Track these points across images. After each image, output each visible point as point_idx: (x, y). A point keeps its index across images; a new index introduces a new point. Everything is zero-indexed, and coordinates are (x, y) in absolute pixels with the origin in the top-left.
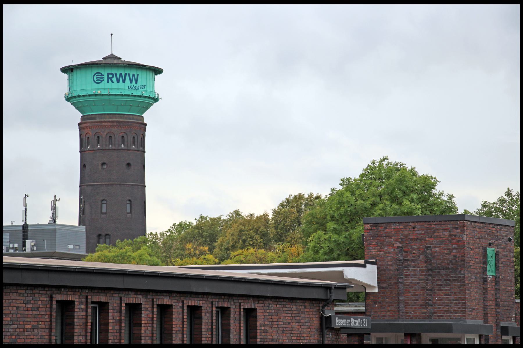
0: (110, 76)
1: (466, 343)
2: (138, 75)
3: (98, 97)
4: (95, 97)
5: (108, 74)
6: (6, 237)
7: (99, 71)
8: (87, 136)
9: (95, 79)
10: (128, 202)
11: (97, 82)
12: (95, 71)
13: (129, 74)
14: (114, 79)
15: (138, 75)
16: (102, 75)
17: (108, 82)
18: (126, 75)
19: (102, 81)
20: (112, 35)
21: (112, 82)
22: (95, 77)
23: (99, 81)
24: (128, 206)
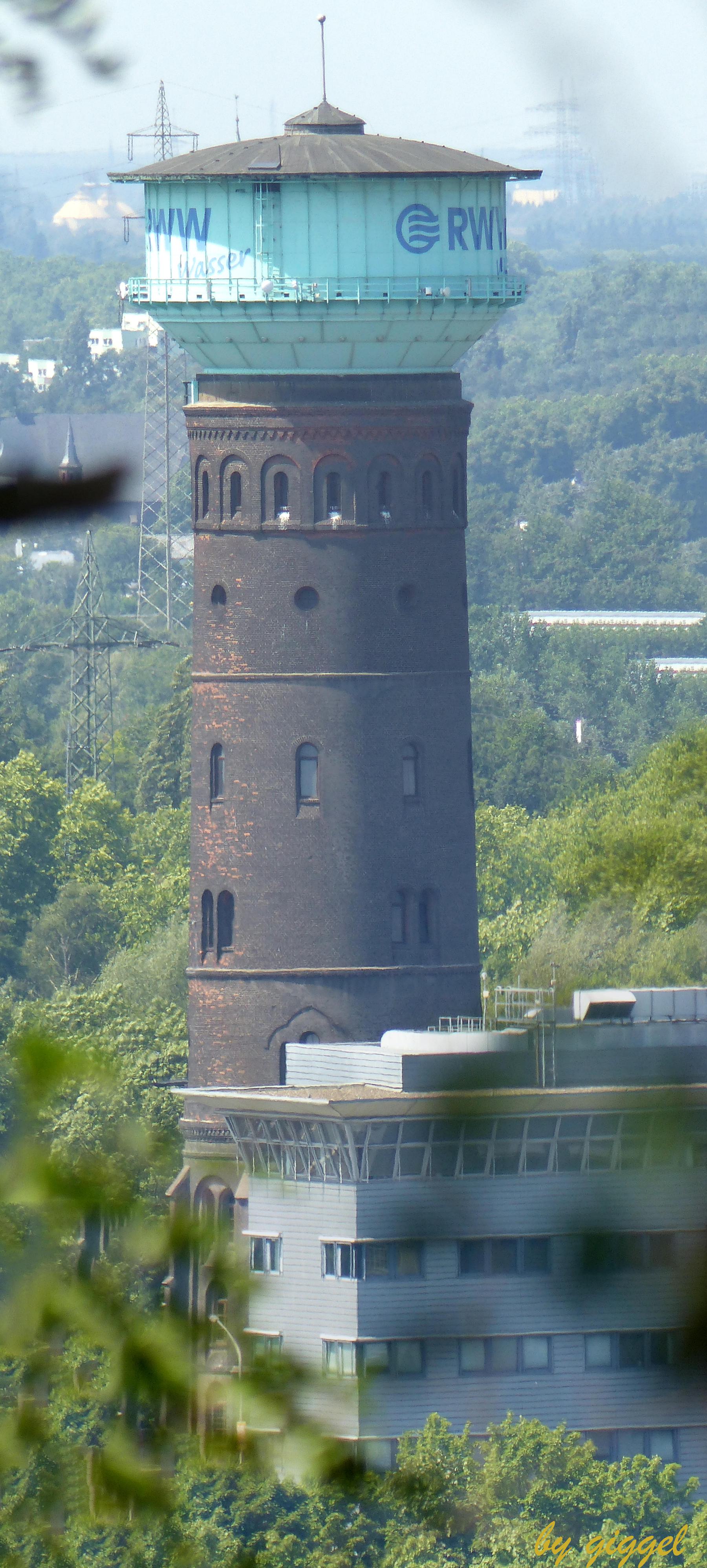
0: (458, 221)
1: (705, 1085)
2: (207, 212)
5: (454, 212)
6: (703, 599)
7: (422, 201)
9: (406, 235)
10: (410, 752)
11: (415, 244)
13: (179, 211)
15: (207, 212)
16: (432, 218)
17: (452, 247)
19: (432, 241)
20: (322, 21)
22: (406, 225)
23: (422, 244)
24: (409, 766)
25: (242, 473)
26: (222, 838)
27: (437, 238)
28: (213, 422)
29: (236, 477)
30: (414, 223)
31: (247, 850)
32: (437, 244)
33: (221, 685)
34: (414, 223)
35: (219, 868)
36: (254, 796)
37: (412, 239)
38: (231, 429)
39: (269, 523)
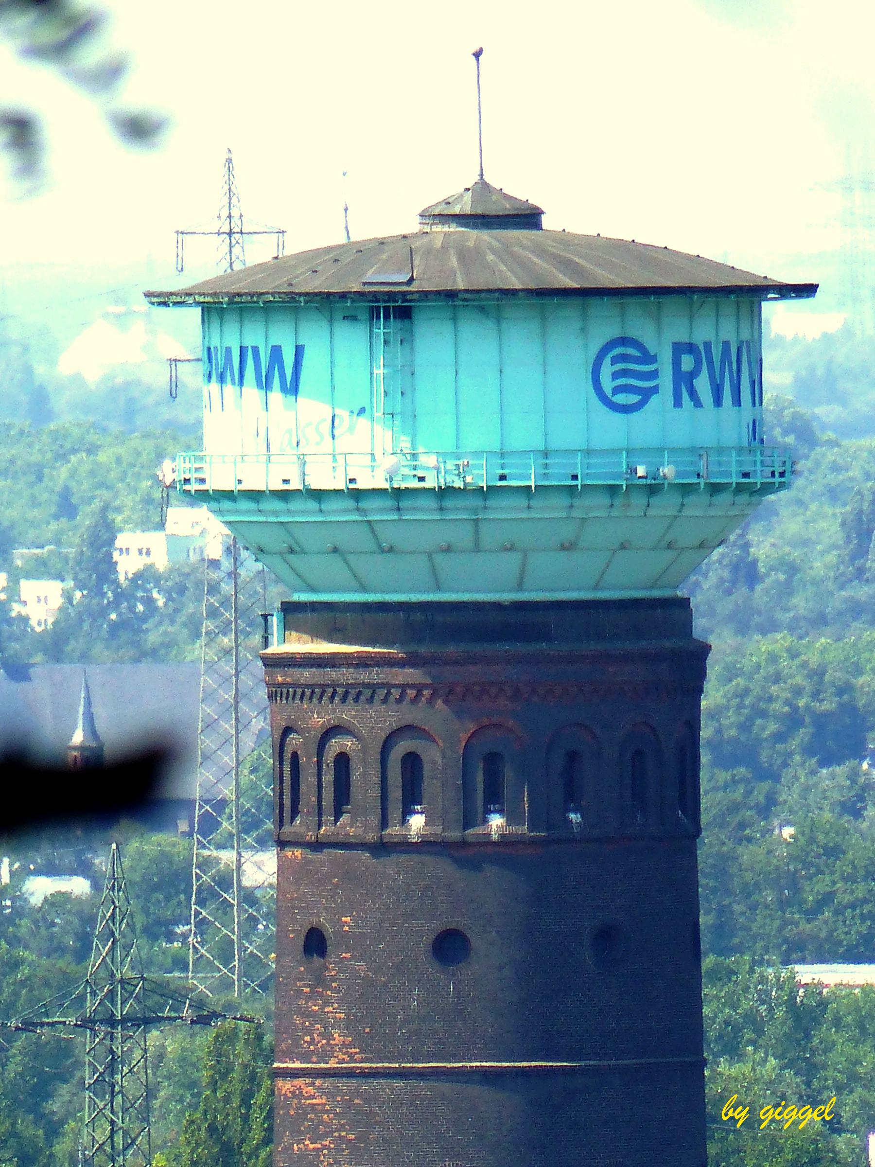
0: (687, 363)
2: (299, 351)
3: (296, 505)
4: (278, 505)
5: (679, 349)
7: (632, 332)
8: (336, 745)
9: (608, 384)
11: (621, 399)
12: (605, 327)
13: (256, 350)
14: (703, 384)
15: (299, 351)
16: (648, 358)
17: (678, 403)
18: (243, 350)
19: (646, 394)
21: (698, 404)
22: (607, 370)
25: (352, 755)
27: (655, 390)
28: (307, 675)
29: (343, 760)
33: (318, 1082)
37: (617, 390)
39: (394, 831)
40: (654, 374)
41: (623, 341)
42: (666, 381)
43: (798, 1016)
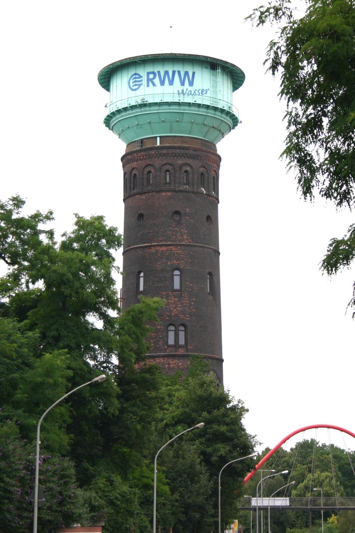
0: (151, 76)
2: (194, 74)
5: (148, 74)
7: (137, 72)
9: (131, 85)
11: (134, 88)
15: (194, 74)
16: (140, 77)
17: (148, 86)
19: (140, 85)
22: (132, 81)
26: (181, 304)
27: (142, 84)
28: (178, 151)
30: (134, 80)
31: (193, 309)
32: (142, 86)
33: (179, 247)
34: (134, 80)
35: (179, 315)
36: (196, 289)
37: (133, 86)
38: (187, 154)
40: (141, 81)
41: (136, 74)
42: (145, 82)
43: (310, 36)
